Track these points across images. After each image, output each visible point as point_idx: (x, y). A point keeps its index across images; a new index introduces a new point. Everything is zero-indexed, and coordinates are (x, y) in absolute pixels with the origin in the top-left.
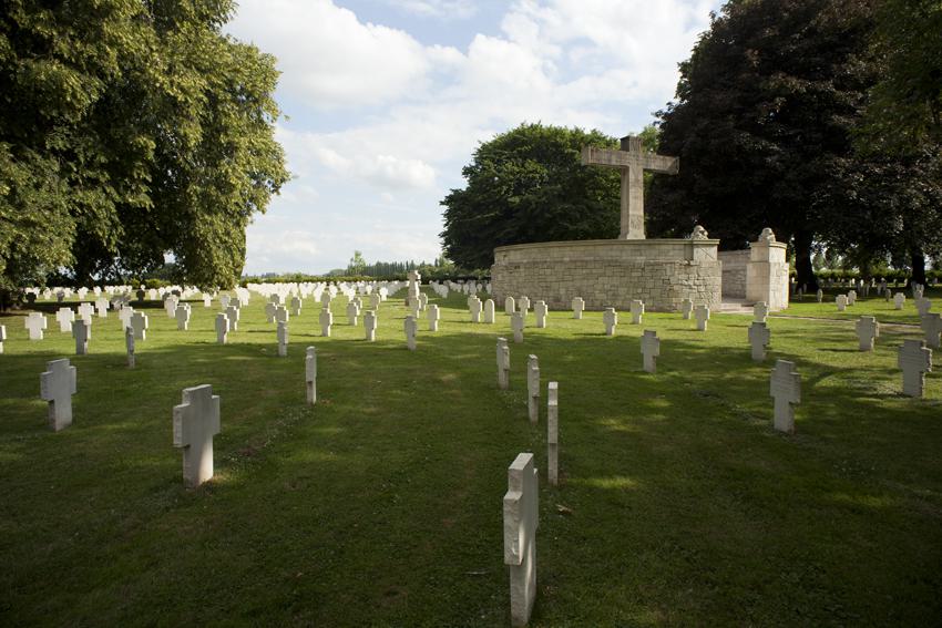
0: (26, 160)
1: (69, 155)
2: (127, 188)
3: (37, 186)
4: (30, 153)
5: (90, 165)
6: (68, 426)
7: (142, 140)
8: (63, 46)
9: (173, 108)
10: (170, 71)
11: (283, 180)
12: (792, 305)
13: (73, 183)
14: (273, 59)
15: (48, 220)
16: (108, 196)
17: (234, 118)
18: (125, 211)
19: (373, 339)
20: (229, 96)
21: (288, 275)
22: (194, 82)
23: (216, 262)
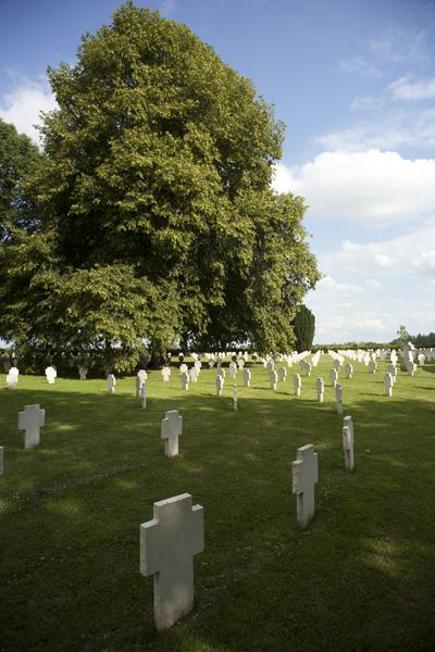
0: (160, 284)
1: (181, 278)
2: (211, 294)
3: (165, 298)
4: (162, 280)
5: (191, 283)
6: (36, 447)
7: (216, 264)
8: (173, 220)
9: (236, 243)
10: (232, 219)
11: (317, 279)
12: (61, 380)
13: (183, 295)
14: (302, 199)
15: (166, 317)
16: (200, 300)
17: (275, 242)
18: (209, 307)
19: (322, 400)
20: (271, 228)
21: (349, 344)
22: (246, 224)
23: (267, 337)
